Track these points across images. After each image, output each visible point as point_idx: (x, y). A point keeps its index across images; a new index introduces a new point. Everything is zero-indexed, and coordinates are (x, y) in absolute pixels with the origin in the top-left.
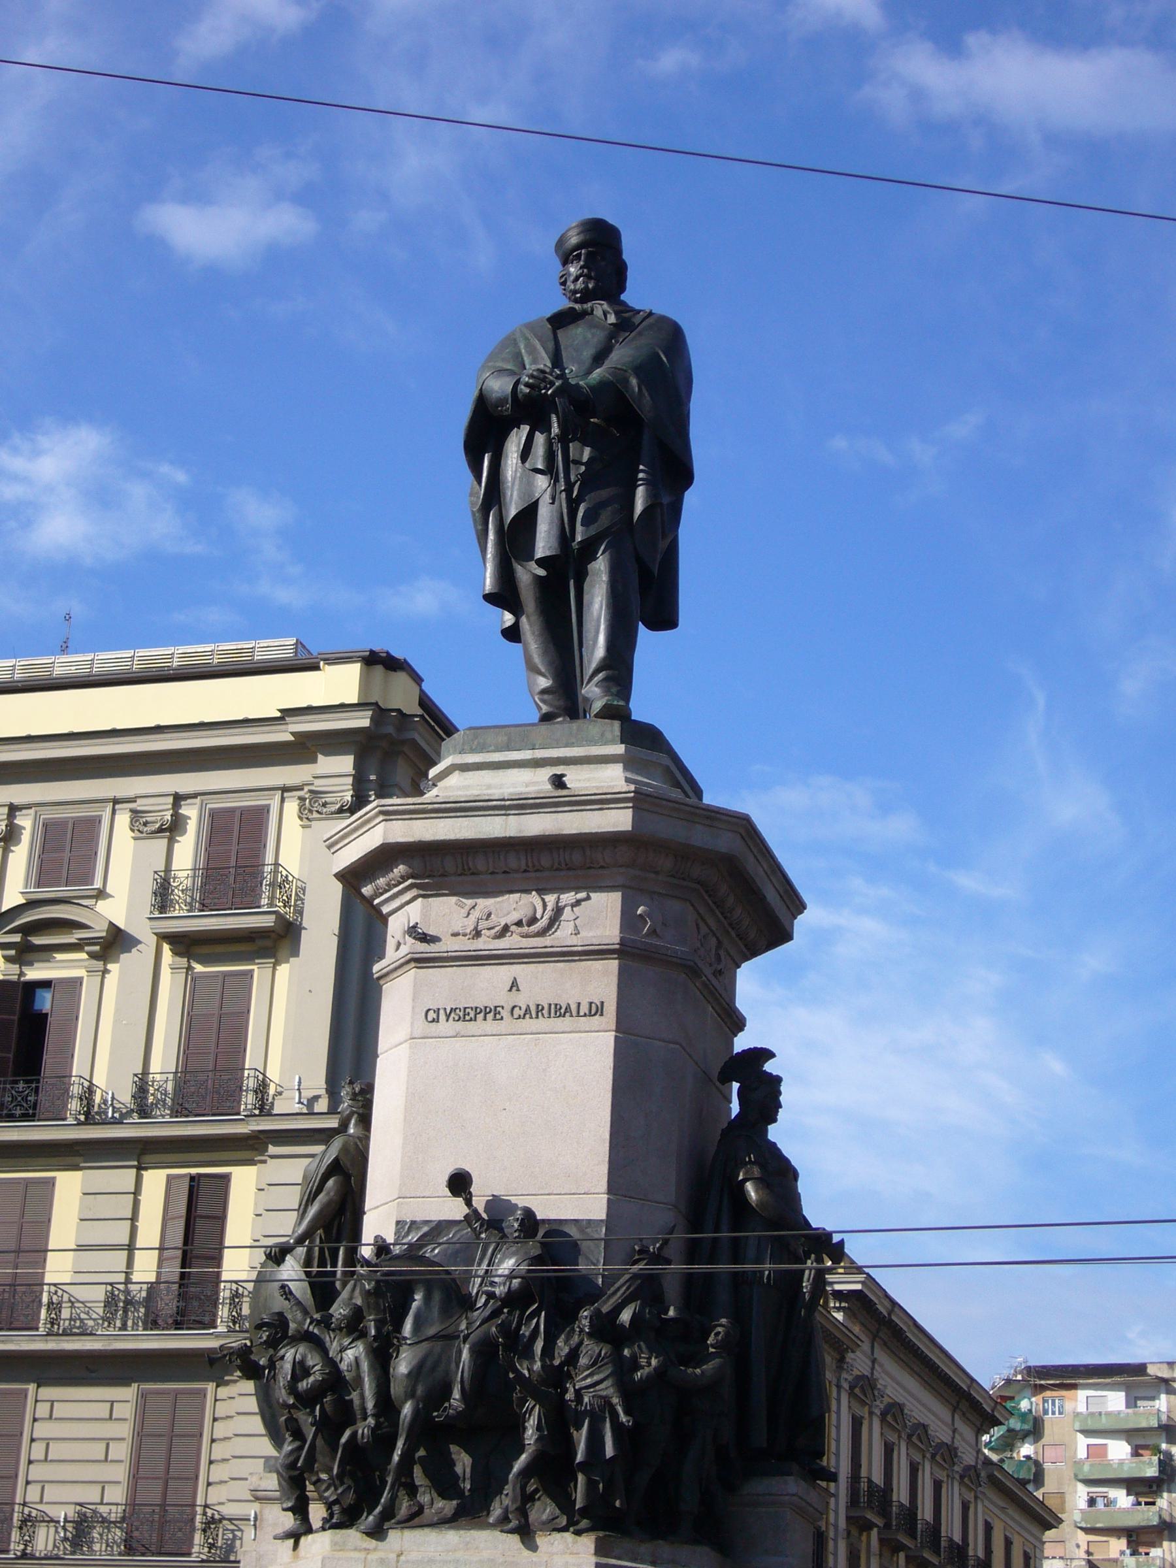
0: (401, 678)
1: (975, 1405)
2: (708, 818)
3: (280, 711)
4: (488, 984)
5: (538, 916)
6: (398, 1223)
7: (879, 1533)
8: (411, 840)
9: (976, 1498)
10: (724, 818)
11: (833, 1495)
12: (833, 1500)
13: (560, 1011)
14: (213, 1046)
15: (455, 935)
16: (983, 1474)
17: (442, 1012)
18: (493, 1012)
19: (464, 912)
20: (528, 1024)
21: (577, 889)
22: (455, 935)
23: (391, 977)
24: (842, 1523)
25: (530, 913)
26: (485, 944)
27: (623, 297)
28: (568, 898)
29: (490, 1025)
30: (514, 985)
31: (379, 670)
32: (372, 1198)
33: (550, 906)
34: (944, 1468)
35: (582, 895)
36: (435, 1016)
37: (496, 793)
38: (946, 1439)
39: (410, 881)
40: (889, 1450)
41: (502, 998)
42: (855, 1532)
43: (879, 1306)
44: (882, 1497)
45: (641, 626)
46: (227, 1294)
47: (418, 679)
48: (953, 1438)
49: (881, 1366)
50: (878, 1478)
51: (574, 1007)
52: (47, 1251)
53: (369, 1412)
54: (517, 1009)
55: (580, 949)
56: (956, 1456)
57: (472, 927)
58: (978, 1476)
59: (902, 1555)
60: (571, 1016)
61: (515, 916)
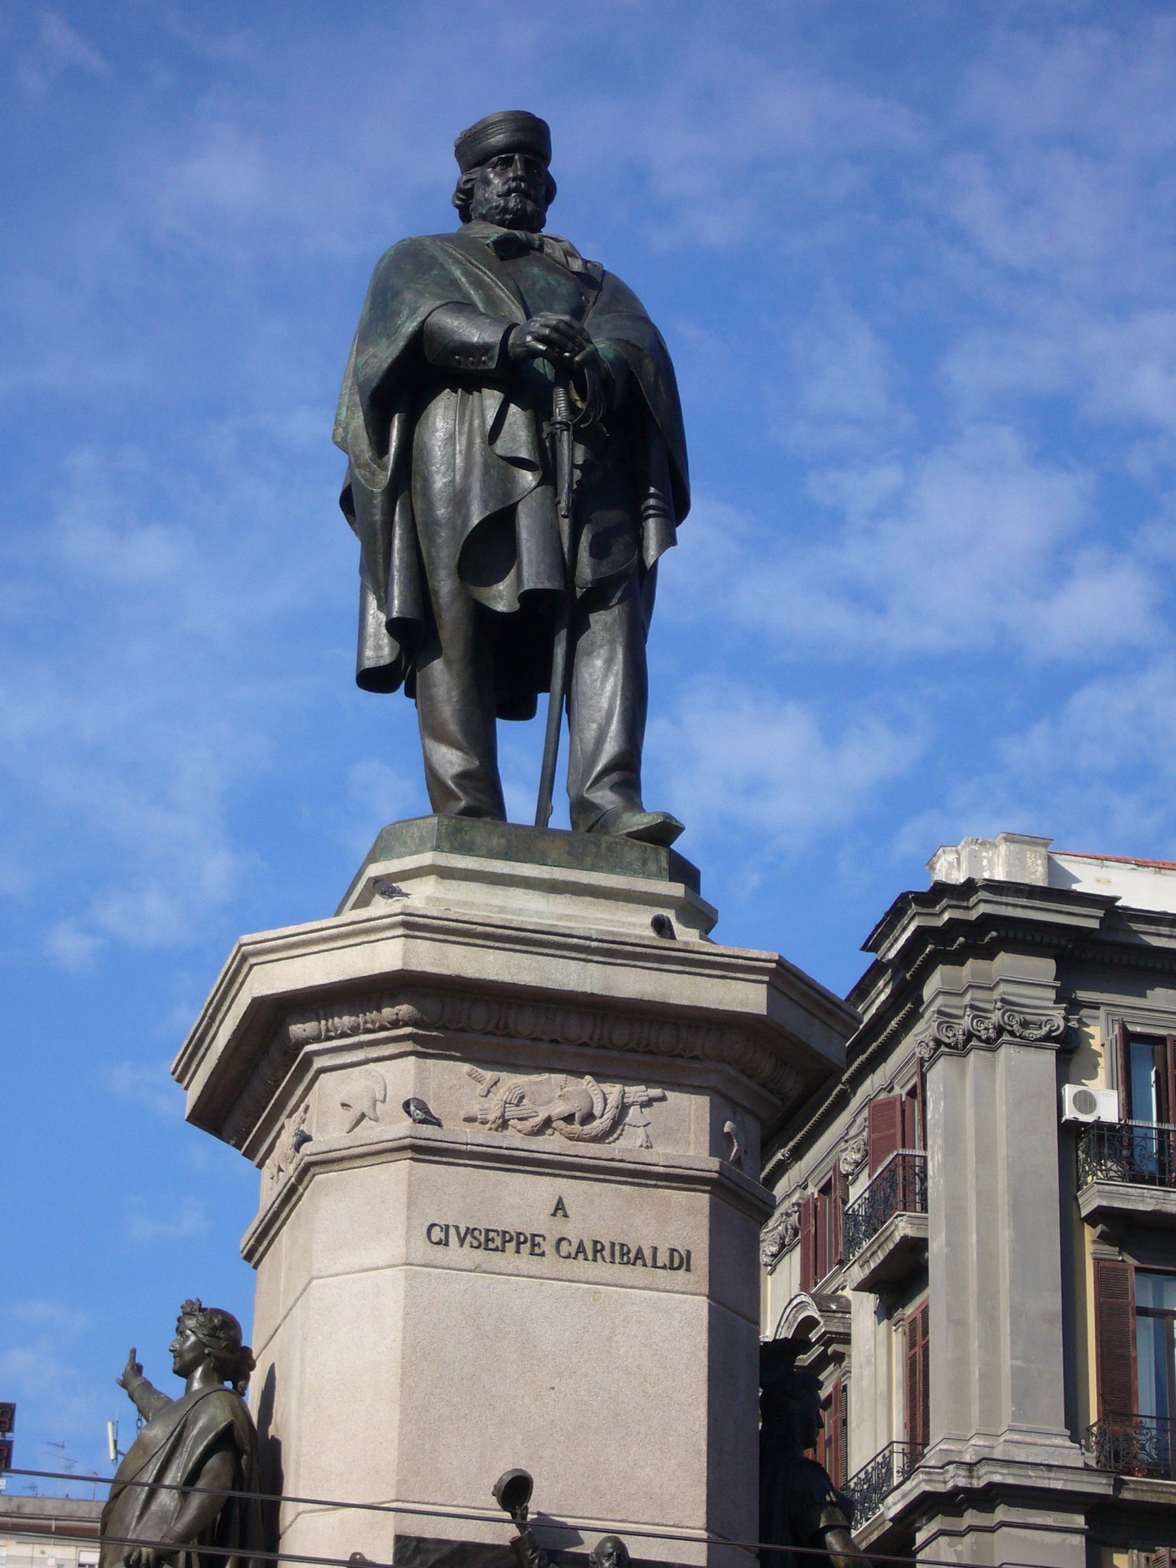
2: (828, 1012)
4: (523, 1200)
5: (597, 1111)
8: (445, 972)
10: (844, 1016)
15: (470, 1120)
17: (452, 1231)
19: (481, 1088)
20: (581, 1267)
21: (649, 1082)
22: (470, 1120)
23: (346, 1165)
25: (586, 1110)
26: (513, 1139)
28: (637, 1092)
29: (524, 1261)
30: (560, 1207)
33: (613, 1100)
35: (656, 1092)
36: (442, 1236)
37: (579, 928)
39: (408, 1030)
41: (539, 1221)
54: (564, 1244)
55: (661, 1170)
57: (498, 1113)
60: (645, 1265)
61: (559, 1108)
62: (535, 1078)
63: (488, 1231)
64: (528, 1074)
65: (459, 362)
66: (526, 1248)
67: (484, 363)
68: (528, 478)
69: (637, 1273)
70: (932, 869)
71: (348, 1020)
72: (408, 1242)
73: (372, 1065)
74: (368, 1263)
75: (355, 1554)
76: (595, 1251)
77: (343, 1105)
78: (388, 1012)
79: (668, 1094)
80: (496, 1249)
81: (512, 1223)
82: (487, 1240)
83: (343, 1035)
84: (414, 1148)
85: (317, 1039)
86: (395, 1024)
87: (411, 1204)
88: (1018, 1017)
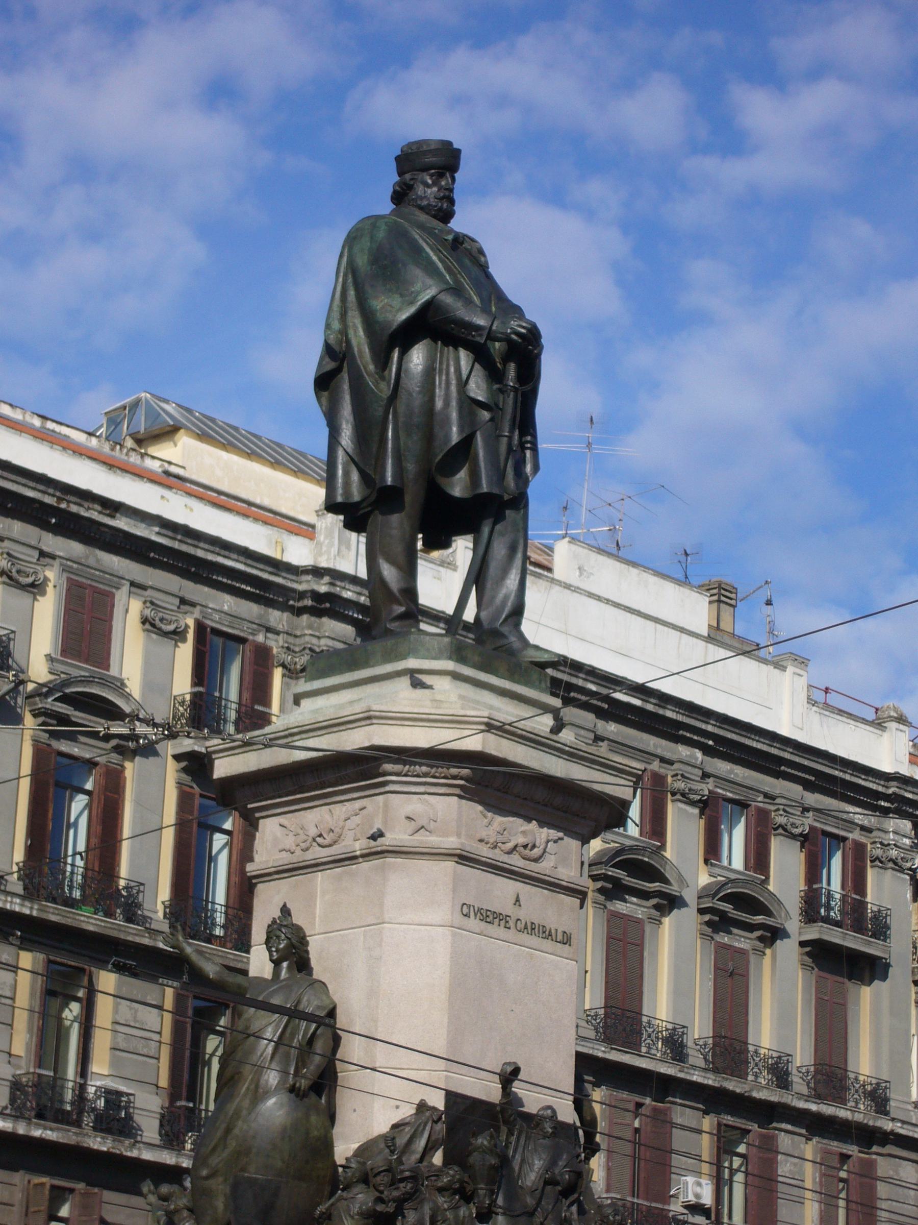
5: (537, 844)
14: (835, 1000)
15: (481, 841)
19: (486, 821)
20: (525, 938)
21: (557, 828)
22: (481, 841)
23: (409, 856)
26: (498, 856)
29: (500, 931)
41: (507, 908)
52: (671, 1151)
61: (521, 840)
62: (511, 819)
63: (487, 910)
64: (505, 816)
65: (453, 329)
66: (503, 923)
67: (473, 336)
68: (486, 415)
69: (548, 944)
71: (424, 769)
72: (452, 913)
73: (426, 796)
74: (424, 921)
75: (422, 1100)
76: (533, 929)
77: (408, 818)
78: (454, 771)
79: (565, 838)
83: (418, 776)
84: (461, 857)
85: (398, 774)
86: (454, 777)
87: (454, 890)
88: (160, 615)
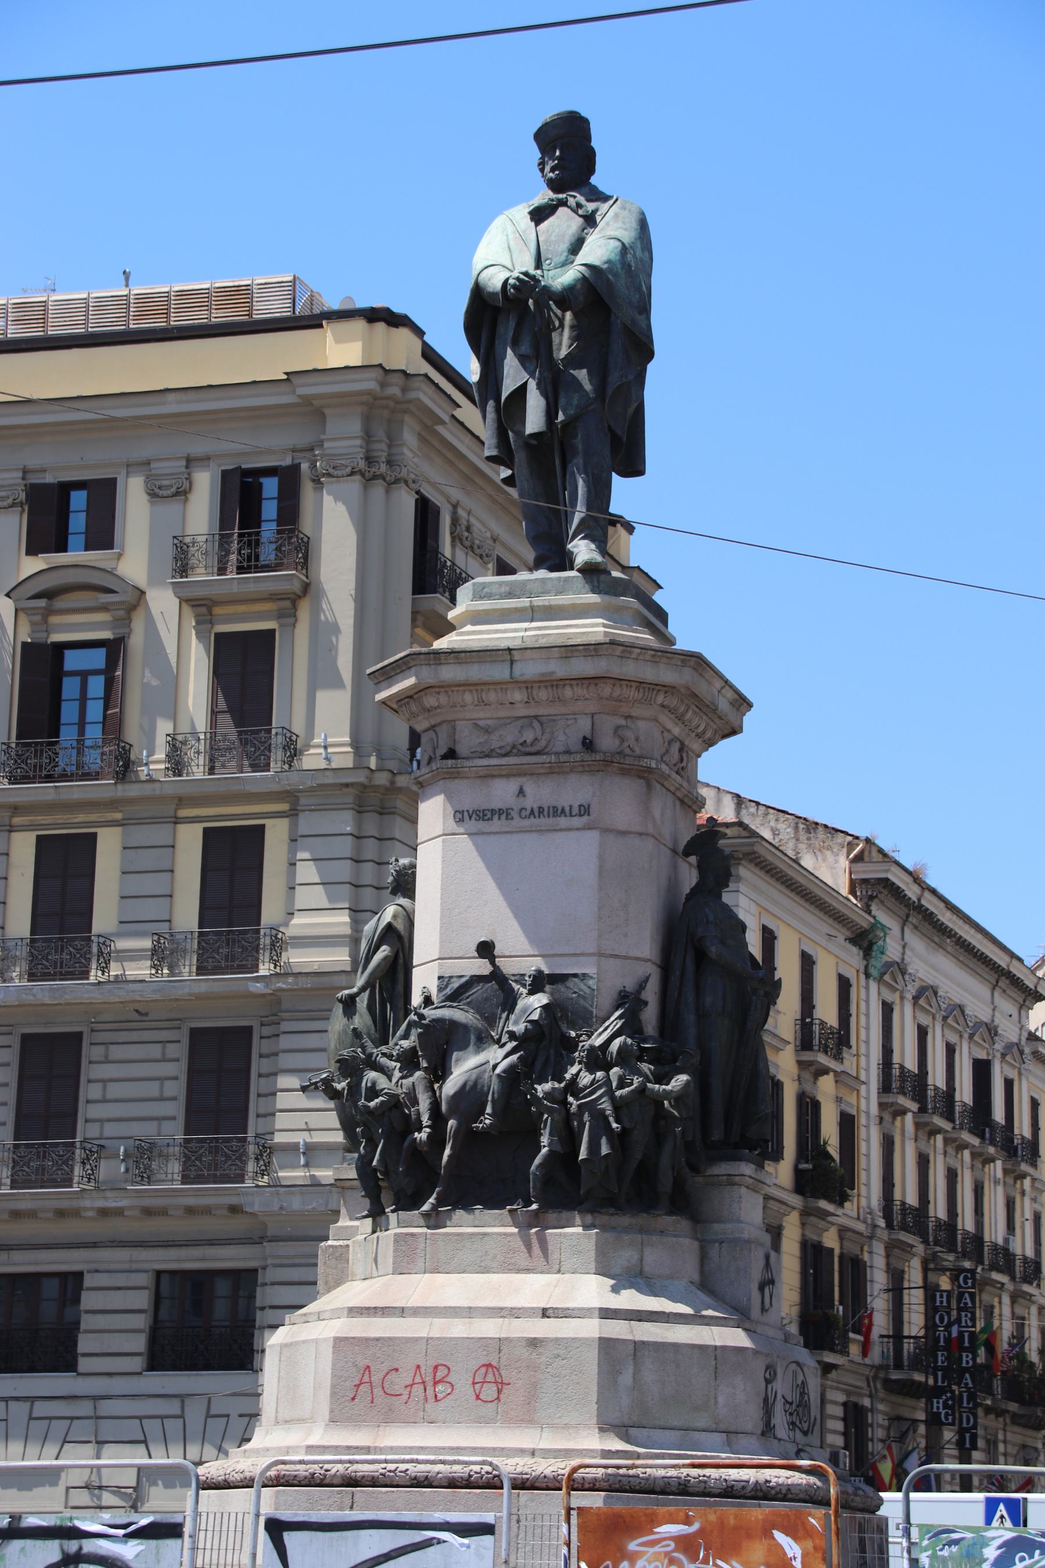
0: (404, 333)
1: (1016, 982)
3: (286, 373)
6: (439, 978)
7: (914, 1117)
9: (1020, 1074)
11: (864, 1083)
12: (863, 1088)
13: (557, 812)
16: (1027, 1050)
18: (504, 813)
24: (874, 1109)
27: (594, 180)
30: (521, 792)
31: (381, 326)
32: (419, 955)
34: (984, 1048)
38: (986, 1018)
40: (922, 1033)
42: (887, 1117)
43: (907, 892)
44: (917, 1084)
45: (614, 474)
46: (268, 941)
47: (419, 332)
48: (993, 1016)
49: (912, 950)
50: (911, 1064)
51: (567, 809)
53: (425, 1124)
56: (996, 1034)
58: (1022, 1053)
59: (939, 1138)
70: (700, 867)
80: (488, 820)
81: (496, 805)
82: (484, 815)
